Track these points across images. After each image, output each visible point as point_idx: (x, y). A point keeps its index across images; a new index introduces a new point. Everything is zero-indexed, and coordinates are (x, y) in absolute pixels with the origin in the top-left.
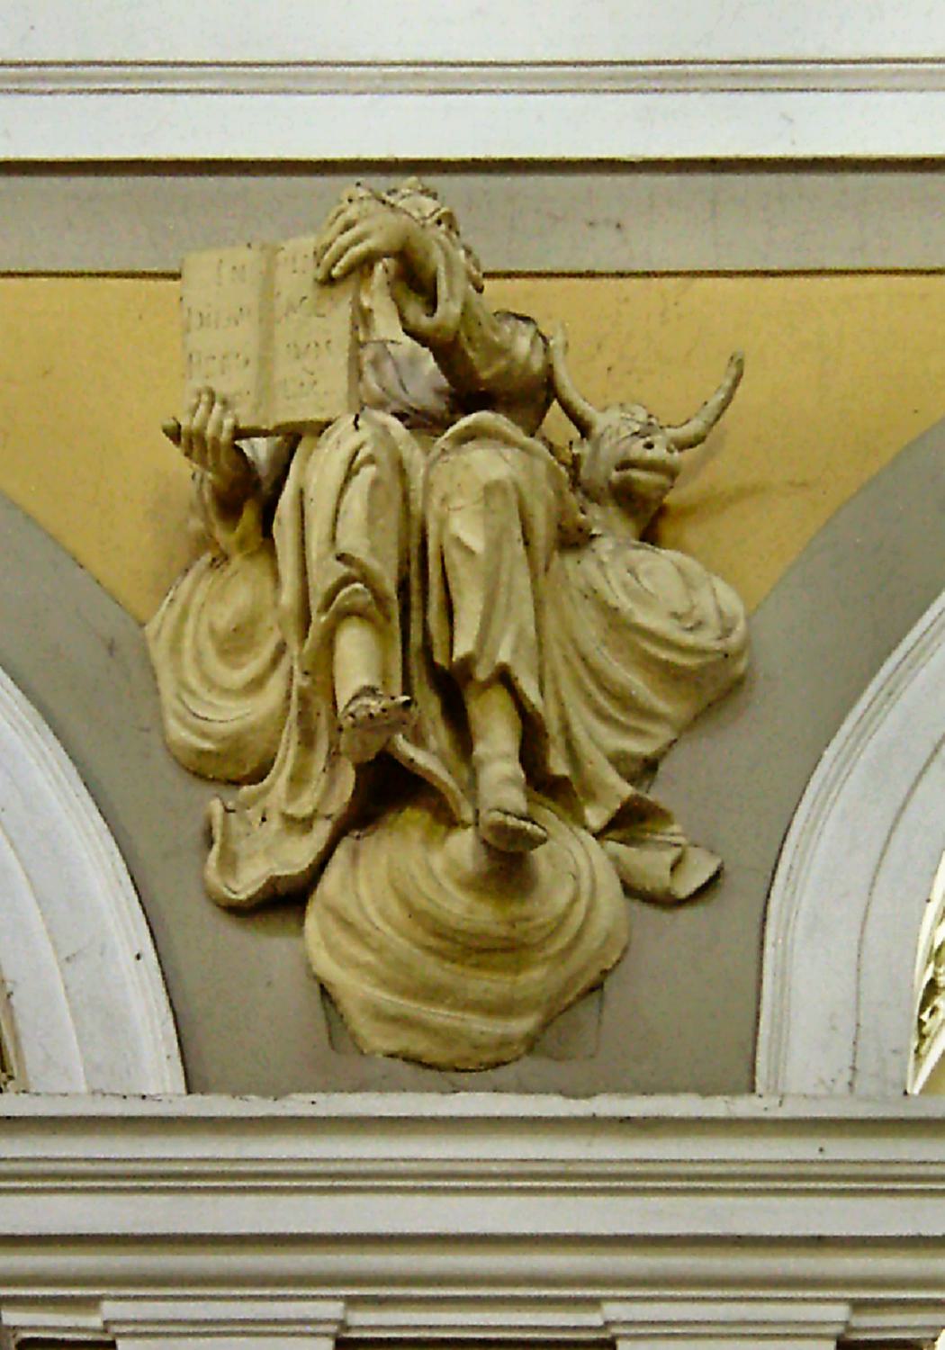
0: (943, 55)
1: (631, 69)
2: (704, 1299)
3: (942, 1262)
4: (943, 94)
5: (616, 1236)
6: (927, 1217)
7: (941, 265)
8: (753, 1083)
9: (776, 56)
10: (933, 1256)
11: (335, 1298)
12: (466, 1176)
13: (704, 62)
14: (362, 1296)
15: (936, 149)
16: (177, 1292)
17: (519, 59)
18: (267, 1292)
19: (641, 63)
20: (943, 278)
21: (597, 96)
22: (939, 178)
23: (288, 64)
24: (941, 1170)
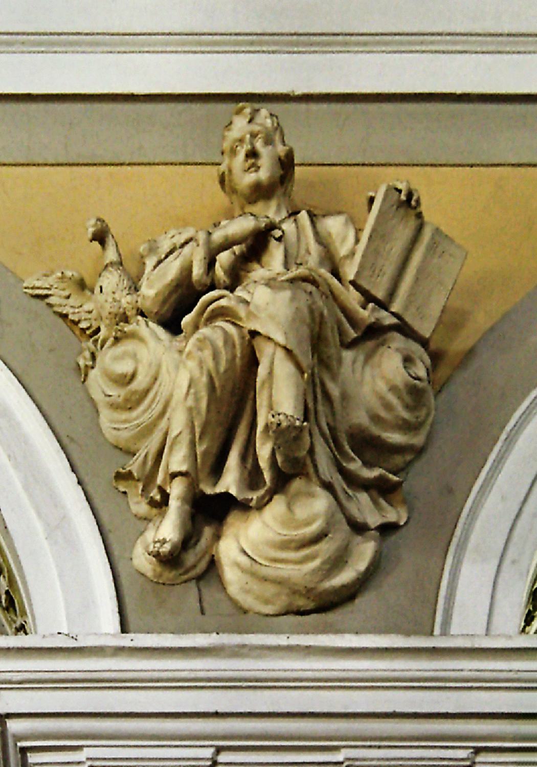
0: (536, 32)
1: (413, 38)
2: (411, 747)
3: (536, 727)
4: (536, 55)
5: (503, 714)
6: (526, 702)
7: (535, 161)
8: (432, 631)
9: (395, 30)
10: (532, 724)
11: (211, 746)
12: (301, 680)
13: (24, 34)
14: (282, 746)
15: (533, 90)
16: (353, 743)
17: (178, 31)
18: (198, 743)
19: (407, 34)
20: (536, 169)
21: (23, 55)
22: (532, 108)
23: (377, 35)
24: (534, 675)
